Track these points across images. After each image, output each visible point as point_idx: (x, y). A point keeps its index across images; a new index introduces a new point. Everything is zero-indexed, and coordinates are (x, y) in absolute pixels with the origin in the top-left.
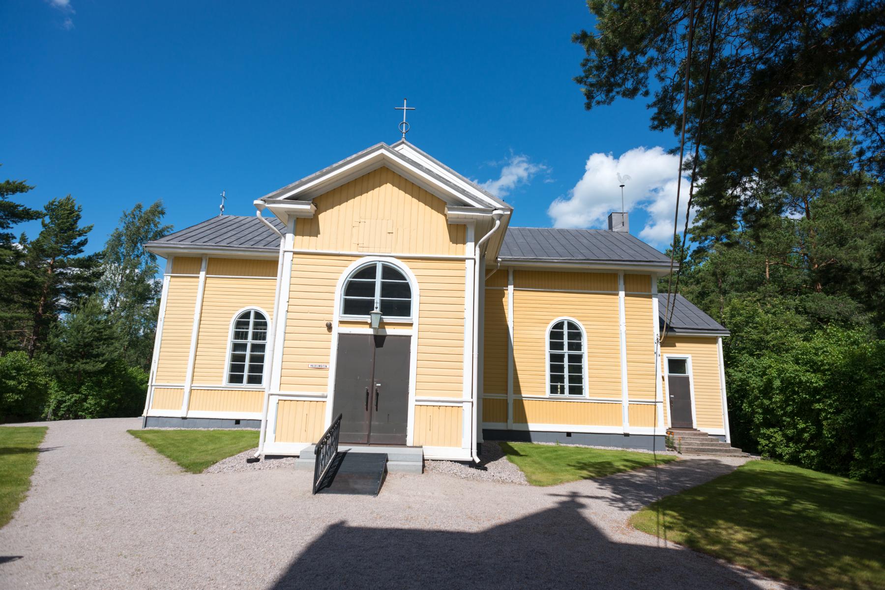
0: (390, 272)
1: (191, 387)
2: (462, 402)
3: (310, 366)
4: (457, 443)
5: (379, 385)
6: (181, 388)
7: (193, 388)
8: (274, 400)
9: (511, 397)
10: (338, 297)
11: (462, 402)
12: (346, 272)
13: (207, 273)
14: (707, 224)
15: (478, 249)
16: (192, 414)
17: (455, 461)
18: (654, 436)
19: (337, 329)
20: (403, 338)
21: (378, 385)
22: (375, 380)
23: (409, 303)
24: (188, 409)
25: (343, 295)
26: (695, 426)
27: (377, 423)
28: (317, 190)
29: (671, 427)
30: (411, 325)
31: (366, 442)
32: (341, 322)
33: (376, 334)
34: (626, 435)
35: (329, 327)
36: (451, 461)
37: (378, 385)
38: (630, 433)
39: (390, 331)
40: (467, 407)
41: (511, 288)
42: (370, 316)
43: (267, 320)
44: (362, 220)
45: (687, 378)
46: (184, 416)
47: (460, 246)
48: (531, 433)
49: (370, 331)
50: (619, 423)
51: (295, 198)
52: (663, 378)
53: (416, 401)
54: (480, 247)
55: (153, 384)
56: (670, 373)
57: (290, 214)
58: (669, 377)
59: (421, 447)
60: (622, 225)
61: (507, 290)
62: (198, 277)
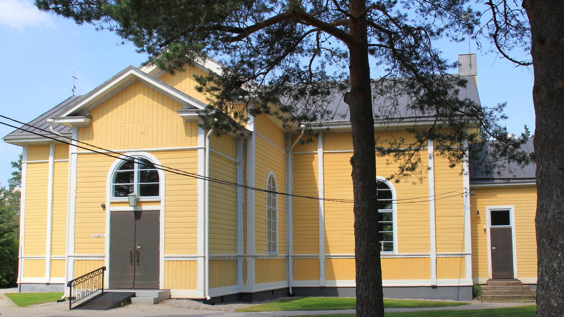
0: (147, 163)
1: (51, 258)
2: (197, 257)
3: (93, 236)
4: (194, 287)
5: (140, 247)
6: (427, 257)
7: (52, 259)
8: (71, 260)
9: (322, 255)
10: (109, 184)
11: (197, 257)
12: (114, 165)
13: (54, 158)
14: (419, 94)
15: (207, 140)
16: (53, 280)
17: (193, 299)
18: (459, 286)
19: (110, 208)
20: (154, 212)
21: (138, 247)
22: (136, 243)
23: (158, 185)
24: (50, 276)
25: (112, 183)
26: (515, 277)
27: (139, 274)
28: (90, 105)
29: (491, 278)
30: (159, 202)
31: (132, 288)
32: (112, 203)
33: (135, 210)
34: (434, 287)
35: (104, 207)
36: (190, 299)
37: (138, 247)
38: (438, 285)
39: (145, 207)
40: (200, 261)
41: (320, 151)
42: (127, 197)
43: (391, 189)
44: (123, 125)
45: (510, 229)
46: (48, 282)
47: (194, 138)
48: (339, 290)
49: (132, 209)
50: (428, 277)
51: (75, 114)
52: (485, 230)
53: (165, 257)
54: (209, 138)
55: (23, 256)
56: (492, 225)
57: (74, 125)
58: (492, 230)
59: (170, 290)
60: (469, 67)
61: (317, 153)
62: (48, 162)
